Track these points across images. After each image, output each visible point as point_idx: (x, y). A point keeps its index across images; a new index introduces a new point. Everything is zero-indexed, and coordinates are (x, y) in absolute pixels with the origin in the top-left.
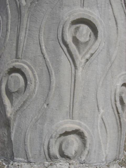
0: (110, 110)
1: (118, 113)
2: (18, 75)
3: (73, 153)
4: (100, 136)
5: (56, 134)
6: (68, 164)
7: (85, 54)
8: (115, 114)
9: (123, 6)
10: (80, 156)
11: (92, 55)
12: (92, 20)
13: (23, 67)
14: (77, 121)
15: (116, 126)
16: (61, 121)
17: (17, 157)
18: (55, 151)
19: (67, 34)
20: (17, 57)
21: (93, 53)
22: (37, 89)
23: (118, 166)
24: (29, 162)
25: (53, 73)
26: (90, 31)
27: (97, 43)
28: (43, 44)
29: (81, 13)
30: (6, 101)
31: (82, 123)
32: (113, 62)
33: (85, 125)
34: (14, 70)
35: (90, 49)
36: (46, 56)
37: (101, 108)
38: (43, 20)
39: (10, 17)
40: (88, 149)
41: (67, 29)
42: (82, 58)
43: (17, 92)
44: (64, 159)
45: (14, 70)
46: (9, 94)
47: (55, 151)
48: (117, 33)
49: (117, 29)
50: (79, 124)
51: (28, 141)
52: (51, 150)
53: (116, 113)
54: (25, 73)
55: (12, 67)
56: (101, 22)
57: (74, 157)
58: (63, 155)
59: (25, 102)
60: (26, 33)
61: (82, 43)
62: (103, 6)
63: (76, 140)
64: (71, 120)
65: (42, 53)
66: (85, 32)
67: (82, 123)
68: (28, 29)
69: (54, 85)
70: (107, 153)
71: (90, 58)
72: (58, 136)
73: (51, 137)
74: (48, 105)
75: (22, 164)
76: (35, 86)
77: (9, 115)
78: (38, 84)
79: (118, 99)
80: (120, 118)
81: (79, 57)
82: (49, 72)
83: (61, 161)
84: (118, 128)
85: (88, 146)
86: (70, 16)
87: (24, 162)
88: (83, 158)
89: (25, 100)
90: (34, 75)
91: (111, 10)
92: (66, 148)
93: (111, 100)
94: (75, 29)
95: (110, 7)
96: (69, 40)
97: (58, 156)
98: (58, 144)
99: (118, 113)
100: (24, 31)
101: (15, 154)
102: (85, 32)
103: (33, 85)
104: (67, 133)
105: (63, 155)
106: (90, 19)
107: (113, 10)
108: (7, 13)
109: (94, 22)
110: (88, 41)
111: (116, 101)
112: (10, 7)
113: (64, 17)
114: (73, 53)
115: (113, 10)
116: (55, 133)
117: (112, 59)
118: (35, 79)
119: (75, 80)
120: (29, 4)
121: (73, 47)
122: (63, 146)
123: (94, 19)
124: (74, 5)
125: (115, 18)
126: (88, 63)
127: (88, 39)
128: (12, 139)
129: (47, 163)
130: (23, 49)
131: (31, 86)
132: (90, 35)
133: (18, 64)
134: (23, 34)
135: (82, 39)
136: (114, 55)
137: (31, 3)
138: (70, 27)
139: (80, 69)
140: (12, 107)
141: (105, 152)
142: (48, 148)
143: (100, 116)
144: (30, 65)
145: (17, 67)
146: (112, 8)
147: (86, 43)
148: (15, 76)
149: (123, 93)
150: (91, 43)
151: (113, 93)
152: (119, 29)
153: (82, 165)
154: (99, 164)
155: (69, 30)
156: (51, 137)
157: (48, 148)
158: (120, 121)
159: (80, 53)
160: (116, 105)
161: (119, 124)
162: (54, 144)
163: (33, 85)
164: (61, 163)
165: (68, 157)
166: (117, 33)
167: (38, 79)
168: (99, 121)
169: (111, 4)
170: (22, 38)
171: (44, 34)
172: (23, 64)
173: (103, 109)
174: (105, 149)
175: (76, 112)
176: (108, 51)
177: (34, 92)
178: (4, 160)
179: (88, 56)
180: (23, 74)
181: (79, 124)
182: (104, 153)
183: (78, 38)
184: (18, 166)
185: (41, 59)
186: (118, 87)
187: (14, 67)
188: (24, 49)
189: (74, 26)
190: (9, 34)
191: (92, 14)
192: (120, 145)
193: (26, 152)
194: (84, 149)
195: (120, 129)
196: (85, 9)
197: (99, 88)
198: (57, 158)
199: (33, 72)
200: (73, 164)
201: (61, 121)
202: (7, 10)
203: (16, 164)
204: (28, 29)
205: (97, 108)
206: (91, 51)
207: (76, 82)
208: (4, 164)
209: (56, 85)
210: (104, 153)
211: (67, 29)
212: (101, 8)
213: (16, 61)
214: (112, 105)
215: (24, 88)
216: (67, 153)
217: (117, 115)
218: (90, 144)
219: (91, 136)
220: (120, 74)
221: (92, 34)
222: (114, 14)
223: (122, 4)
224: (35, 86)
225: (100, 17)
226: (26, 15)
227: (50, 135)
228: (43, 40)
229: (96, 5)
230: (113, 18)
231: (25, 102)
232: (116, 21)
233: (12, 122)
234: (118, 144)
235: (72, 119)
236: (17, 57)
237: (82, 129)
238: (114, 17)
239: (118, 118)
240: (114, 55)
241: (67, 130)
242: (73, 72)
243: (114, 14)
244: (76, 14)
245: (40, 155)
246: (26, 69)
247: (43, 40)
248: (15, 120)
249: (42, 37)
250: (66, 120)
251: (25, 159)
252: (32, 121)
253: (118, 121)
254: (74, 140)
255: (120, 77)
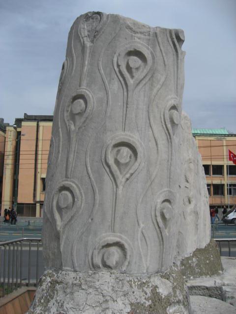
0: (151, 225)
1: (159, 228)
2: (67, 193)
3: (114, 263)
4: (141, 249)
5: (99, 246)
6: (109, 273)
7: (126, 174)
8: (156, 229)
9: (163, 127)
10: (121, 266)
11: (132, 175)
12: (131, 143)
13: (72, 186)
14: (119, 234)
15: (157, 239)
16: (104, 234)
17: (65, 266)
18: (98, 261)
19: (109, 157)
20: (67, 177)
21: (132, 172)
22: (83, 206)
23: (160, 278)
24: (75, 271)
25: (97, 191)
26: (130, 152)
27: (137, 164)
28: (89, 165)
29: (122, 137)
30: (57, 216)
31: (123, 236)
32: (154, 180)
33: (125, 238)
34: (65, 188)
35: (130, 169)
36: (91, 176)
37: (141, 223)
38: (156, 94)
39: (61, 140)
40: (128, 260)
41: (109, 152)
42: (122, 178)
43: (66, 208)
44: (106, 268)
45: (65, 188)
46: (60, 209)
47: (98, 261)
48: (158, 153)
49: (158, 149)
50: (120, 237)
51: (75, 252)
52: (94, 259)
53: (157, 227)
54: (73, 191)
55: (62, 185)
56: (141, 144)
57: (116, 268)
58: (106, 266)
59: (72, 217)
60: (74, 156)
61: (123, 164)
62: (143, 129)
63: (117, 251)
64: (112, 233)
65: (88, 174)
66: (125, 154)
67: (123, 236)
68: (76, 152)
69: (97, 202)
70: (148, 265)
71: (130, 177)
72: (101, 247)
73: (95, 249)
74: (92, 219)
75: (70, 272)
76: (82, 202)
77: (58, 228)
78: (84, 201)
79: (158, 214)
80: (161, 233)
81: (120, 177)
82: (93, 190)
83: (104, 270)
84: (160, 242)
85: (128, 257)
86: (112, 140)
87: (71, 271)
88: (124, 269)
89: (72, 215)
90: (81, 193)
91: (151, 132)
92: (108, 258)
93: (151, 215)
94: (117, 151)
95: (150, 130)
96: (111, 161)
97: (101, 265)
98: (101, 255)
99: (159, 228)
100: (73, 153)
101: (63, 264)
102: (125, 154)
103: (80, 202)
104: (108, 245)
105: (106, 266)
106: (130, 142)
107: (153, 132)
108: (59, 136)
109: (134, 145)
110: (128, 163)
111: (156, 216)
112: (62, 131)
113: (107, 141)
114: (114, 173)
115: (153, 132)
116: (98, 244)
117: (153, 178)
118: (82, 197)
119: (116, 198)
120: (77, 129)
121: (114, 167)
122: (105, 257)
123: (134, 142)
124: (116, 130)
125: (155, 140)
126: (128, 181)
127: (128, 160)
128: (61, 250)
129: (91, 272)
130: (71, 169)
131: (78, 203)
132: (130, 157)
133: (67, 183)
134: (72, 156)
135: (122, 161)
136: (154, 174)
137: (79, 129)
138: (112, 150)
139: (121, 187)
140: (61, 222)
141: (146, 264)
142: (92, 259)
143: (140, 229)
144: (77, 183)
145: (66, 186)
146: (152, 131)
147: (127, 164)
148: (65, 194)
149: (164, 209)
150: (131, 163)
151: (153, 208)
152: (159, 149)
153: (122, 275)
154: (140, 275)
155: (111, 152)
156: (95, 249)
157: (92, 259)
158: (162, 235)
159: (121, 173)
160: (156, 220)
161: (161, 238)
162: (97, 255)
163: (80, 202)
164: (103, 272)
165: (109, 267)
166: (158, 153)
167: (84, 197)
168: (140, 234)
169: (151, 127)
170: (71, 160)
171: (90, 156)
172: (71, 183)
173: (143, 223)
174: (146, 261)
175: (117, 226)
176: (148, 171)
177: (80, 208)
178: (55, 270)
179: (128, 176)
180: (71, 192)
181: (120, 237)
182: (145, 265)
183: (119, 160)
184: (66, 274)
185: (87, 178)
186: (158, 203)
187: (64, 185)
188: (73, 169)
189: (116, 149)
190: (60, 155)
191: (132, 137)
192: (162, 258)
193: (73, 262)
194: (125, 260)
195: (162, 243)
196: (127, 133)
197: (139, 205)
198: (99, 268)
199: (80, 190)
200: (114, 273)
201: (104, 234)
202: (59, 132)
203: (64, 272)
204: (76, 152)
205: (137, 223)
206: (131, 171)
207: (117, 198)
208: (54, 273)
209: (99, 202)
210: (145, 265)
211: (109, 152)
212: (141, 131)
213: (65, 180)
214: (152, 220)
215: (72, 204)
216: (109, 263)
217: (158, 229)
218: (130, 256)
219: (132, 249)
220: (161, 191)
221: (133, 157)
222: (154, 135)
223: (162, 125)
224: (82, 202)
225: (140, 140)
226: (74, 139)
227: (94, 247)
228: (88, 161)
229: (136, 129)
230: (154, 139)
231: (72, 217)
232: (156, 142)
233: (61, 234)
234: (160, 257)
235: (114, 232)
236: (67, 177)
237: (123, 242)
238: (155, 138)
239: (159, 232)
240: (154, 174)
241: (109, 242)
242: (115, 190)
243: (154, 135)
244: (117, 138)
245: (85, 264)
246: (74, 187)
247: (88, 161)
248: (64, 232)
249: (88, 159)
250: (108, 233)
251: (72, 268)
252: (78, 233)
253: (160, 235)
254: (115, 251)
255: (161, 193)
